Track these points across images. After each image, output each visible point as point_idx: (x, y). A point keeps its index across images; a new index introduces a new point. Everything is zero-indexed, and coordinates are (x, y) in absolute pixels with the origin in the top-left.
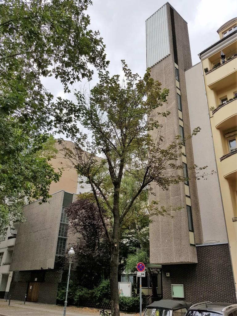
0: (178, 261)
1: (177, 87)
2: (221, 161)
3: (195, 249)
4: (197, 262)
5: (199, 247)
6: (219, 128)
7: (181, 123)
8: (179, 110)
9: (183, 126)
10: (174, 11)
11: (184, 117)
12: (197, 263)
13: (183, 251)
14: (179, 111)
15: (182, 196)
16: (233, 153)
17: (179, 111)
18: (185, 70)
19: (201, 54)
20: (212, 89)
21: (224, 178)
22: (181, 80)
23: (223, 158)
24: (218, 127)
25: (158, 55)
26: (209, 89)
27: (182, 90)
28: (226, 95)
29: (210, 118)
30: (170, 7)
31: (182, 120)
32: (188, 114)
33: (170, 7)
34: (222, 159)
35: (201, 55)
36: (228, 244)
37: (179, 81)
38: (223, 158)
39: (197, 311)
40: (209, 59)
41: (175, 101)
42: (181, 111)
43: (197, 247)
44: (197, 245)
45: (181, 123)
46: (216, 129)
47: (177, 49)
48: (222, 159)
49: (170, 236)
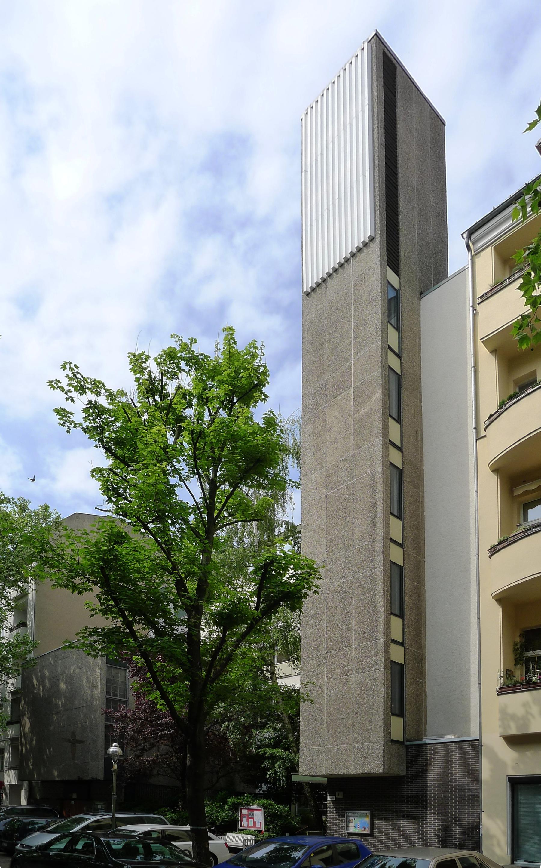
0: (360, 772)
1: (390, 348)
2: (490, 557)
3: (403, 751)
4: (404, 774)
5: (411, 745)
6: (496, 469)
7: (396, 457)
8: (390, 419)
9: (400, 466)
10: (398, 69)
11: (405, 439)
12: (404, 776)
13: (373, 753)
14: (391, 422)
15: (381, 642)
16: (528, 532)
17: (391, 421)
18: (421, 293)
19: (471, 232)
20: (494, 352)
21: (493, 597)
22: (405, 325)
23: (499, 547)
24: (495, 467)
25: (314, 218)
26: (483, 350)
27: (404, 356)
28: (534, 369)
29: (477, 440)
30: (384, 54)
31: (399, 449)
32: (419, 432)
33: (384, 54)
34: (494, 550)
35: (474, 236)
36: (478, 740)
37: (398, 328)
38: (499, 547)
39: (150, 529)
40: (497, 250)
41: (380, 391)
42: (399, 420)
43: (407, 746)
44: (407, 741)
45: (396, 457)
46: (491, 472)
47: (400, 217)
48: (494, 550)
49: (345, 725)
